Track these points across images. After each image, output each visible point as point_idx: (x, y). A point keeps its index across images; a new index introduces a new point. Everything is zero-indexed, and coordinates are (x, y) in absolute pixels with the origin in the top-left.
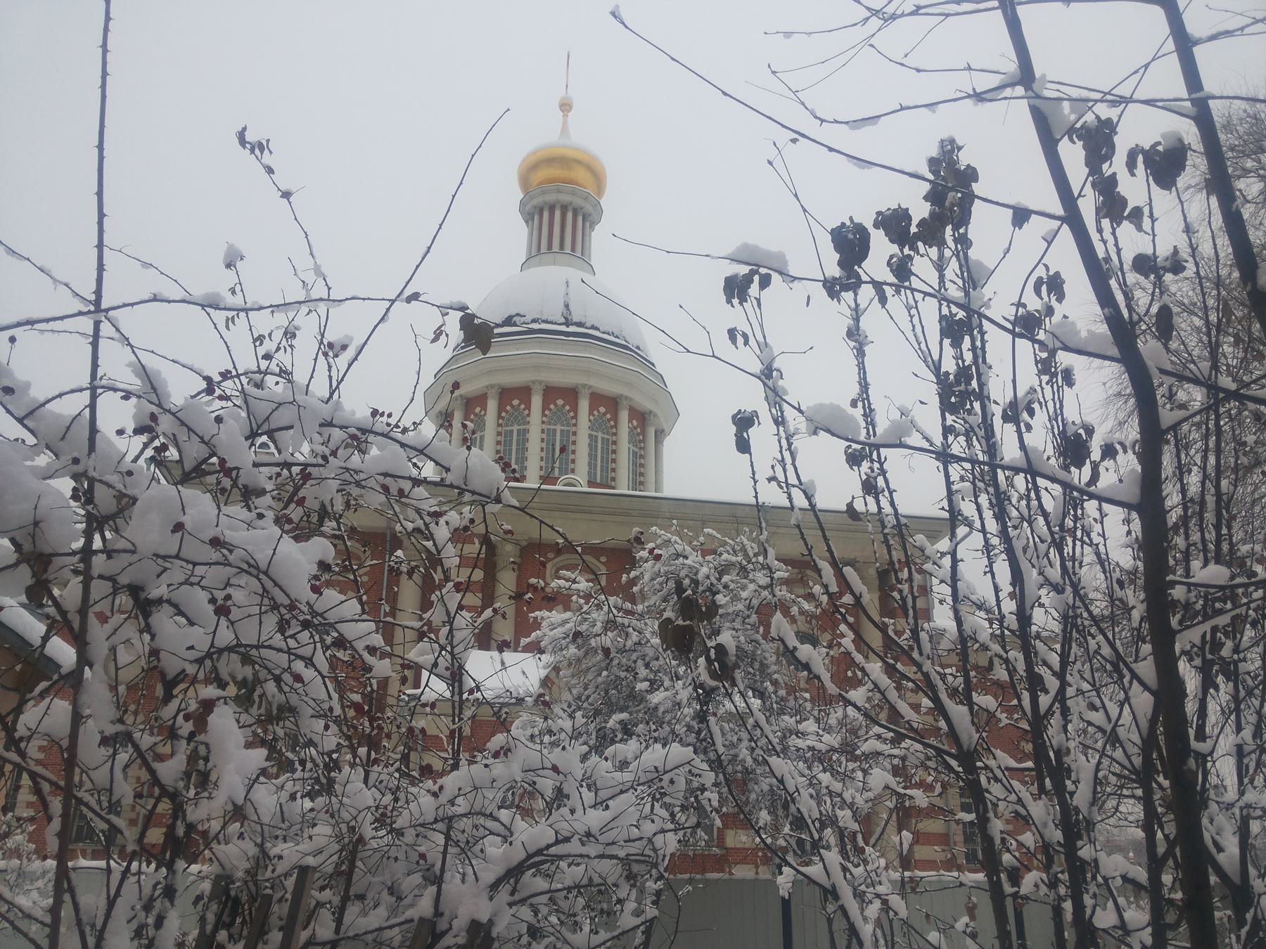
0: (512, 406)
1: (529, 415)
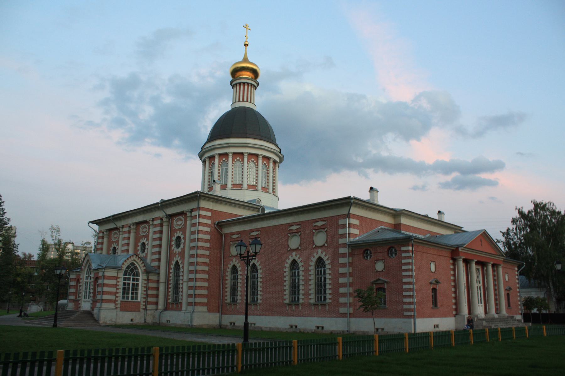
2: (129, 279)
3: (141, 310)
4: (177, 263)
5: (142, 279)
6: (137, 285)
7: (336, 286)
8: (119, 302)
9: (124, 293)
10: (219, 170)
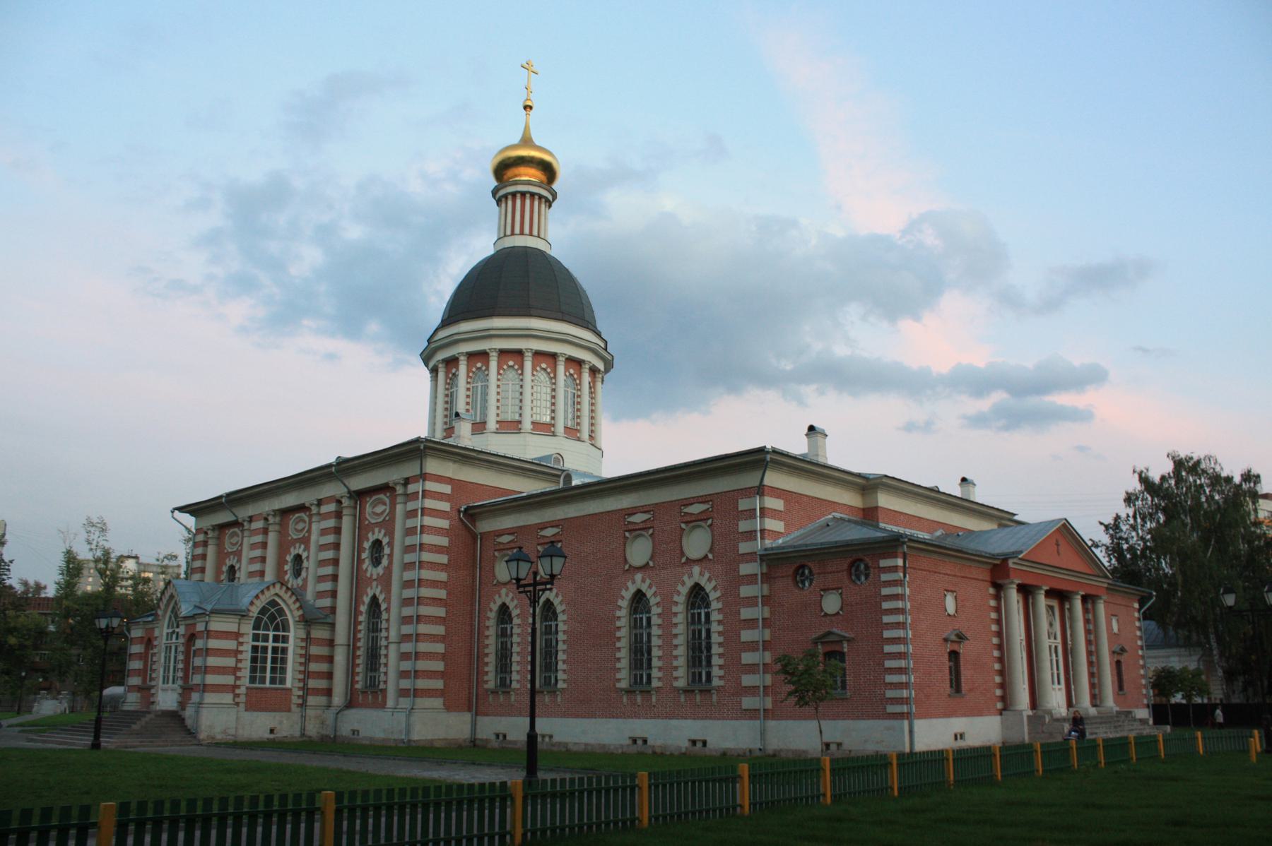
2: (266, 639)
3: (294, 708)
4: (374, 601)
6: (284, 650)
7: (735, 647)
8: (242, 690)
9: (253, 670)
10: (468, 389)
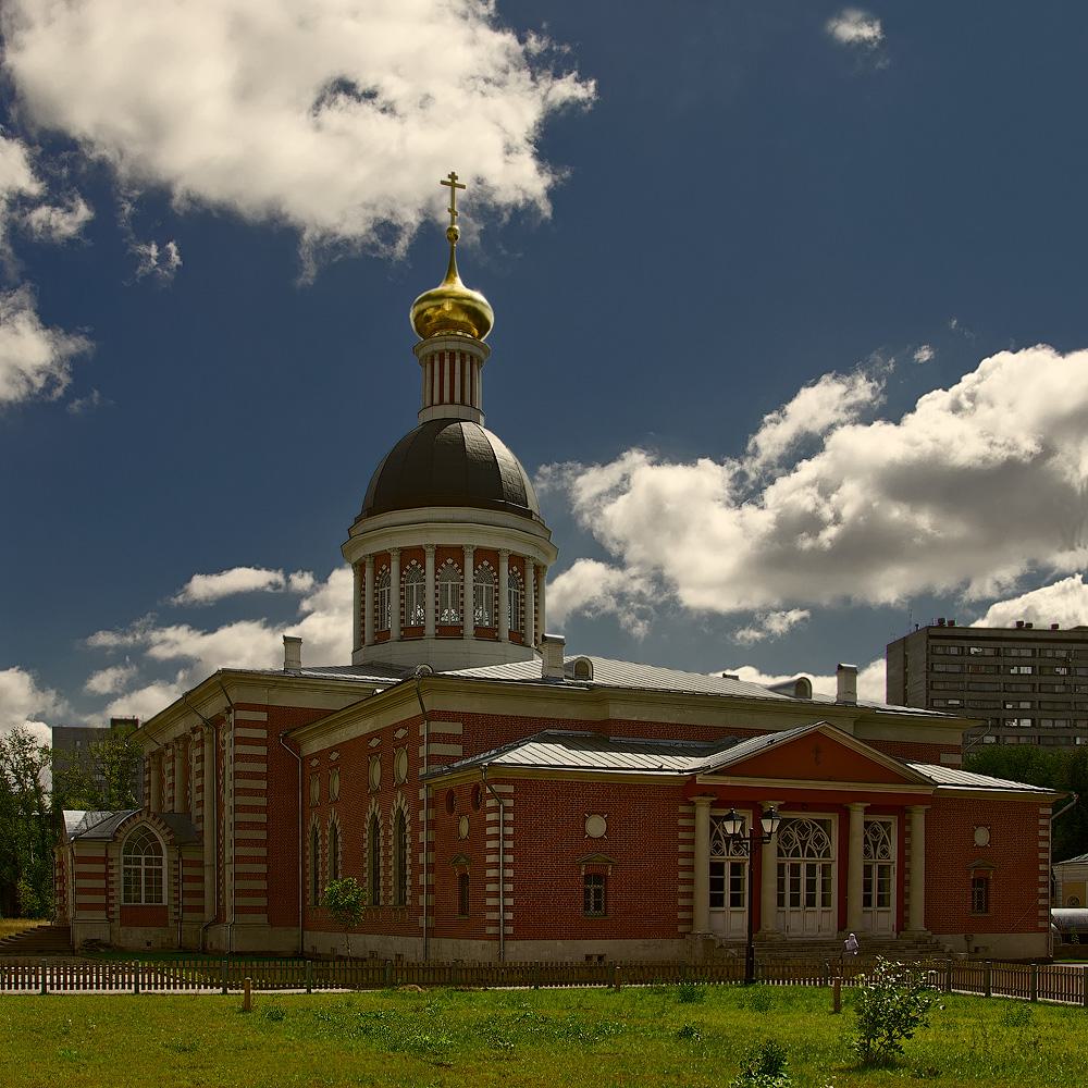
0: (411, 566)
1: (424, 574)
2: (138, 862)
5: (169, 861)
10: (402, 590)
